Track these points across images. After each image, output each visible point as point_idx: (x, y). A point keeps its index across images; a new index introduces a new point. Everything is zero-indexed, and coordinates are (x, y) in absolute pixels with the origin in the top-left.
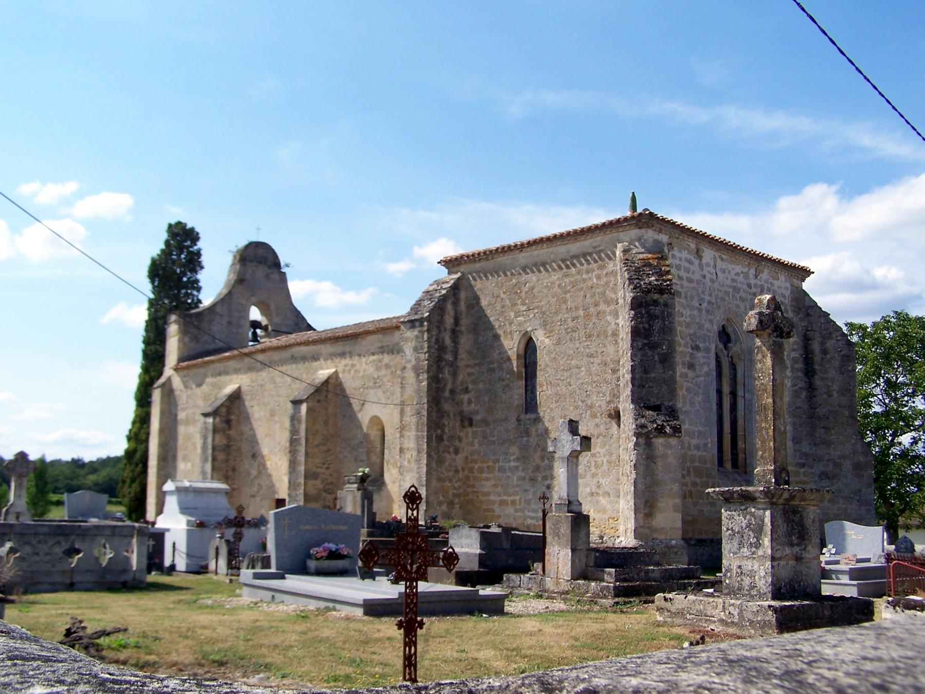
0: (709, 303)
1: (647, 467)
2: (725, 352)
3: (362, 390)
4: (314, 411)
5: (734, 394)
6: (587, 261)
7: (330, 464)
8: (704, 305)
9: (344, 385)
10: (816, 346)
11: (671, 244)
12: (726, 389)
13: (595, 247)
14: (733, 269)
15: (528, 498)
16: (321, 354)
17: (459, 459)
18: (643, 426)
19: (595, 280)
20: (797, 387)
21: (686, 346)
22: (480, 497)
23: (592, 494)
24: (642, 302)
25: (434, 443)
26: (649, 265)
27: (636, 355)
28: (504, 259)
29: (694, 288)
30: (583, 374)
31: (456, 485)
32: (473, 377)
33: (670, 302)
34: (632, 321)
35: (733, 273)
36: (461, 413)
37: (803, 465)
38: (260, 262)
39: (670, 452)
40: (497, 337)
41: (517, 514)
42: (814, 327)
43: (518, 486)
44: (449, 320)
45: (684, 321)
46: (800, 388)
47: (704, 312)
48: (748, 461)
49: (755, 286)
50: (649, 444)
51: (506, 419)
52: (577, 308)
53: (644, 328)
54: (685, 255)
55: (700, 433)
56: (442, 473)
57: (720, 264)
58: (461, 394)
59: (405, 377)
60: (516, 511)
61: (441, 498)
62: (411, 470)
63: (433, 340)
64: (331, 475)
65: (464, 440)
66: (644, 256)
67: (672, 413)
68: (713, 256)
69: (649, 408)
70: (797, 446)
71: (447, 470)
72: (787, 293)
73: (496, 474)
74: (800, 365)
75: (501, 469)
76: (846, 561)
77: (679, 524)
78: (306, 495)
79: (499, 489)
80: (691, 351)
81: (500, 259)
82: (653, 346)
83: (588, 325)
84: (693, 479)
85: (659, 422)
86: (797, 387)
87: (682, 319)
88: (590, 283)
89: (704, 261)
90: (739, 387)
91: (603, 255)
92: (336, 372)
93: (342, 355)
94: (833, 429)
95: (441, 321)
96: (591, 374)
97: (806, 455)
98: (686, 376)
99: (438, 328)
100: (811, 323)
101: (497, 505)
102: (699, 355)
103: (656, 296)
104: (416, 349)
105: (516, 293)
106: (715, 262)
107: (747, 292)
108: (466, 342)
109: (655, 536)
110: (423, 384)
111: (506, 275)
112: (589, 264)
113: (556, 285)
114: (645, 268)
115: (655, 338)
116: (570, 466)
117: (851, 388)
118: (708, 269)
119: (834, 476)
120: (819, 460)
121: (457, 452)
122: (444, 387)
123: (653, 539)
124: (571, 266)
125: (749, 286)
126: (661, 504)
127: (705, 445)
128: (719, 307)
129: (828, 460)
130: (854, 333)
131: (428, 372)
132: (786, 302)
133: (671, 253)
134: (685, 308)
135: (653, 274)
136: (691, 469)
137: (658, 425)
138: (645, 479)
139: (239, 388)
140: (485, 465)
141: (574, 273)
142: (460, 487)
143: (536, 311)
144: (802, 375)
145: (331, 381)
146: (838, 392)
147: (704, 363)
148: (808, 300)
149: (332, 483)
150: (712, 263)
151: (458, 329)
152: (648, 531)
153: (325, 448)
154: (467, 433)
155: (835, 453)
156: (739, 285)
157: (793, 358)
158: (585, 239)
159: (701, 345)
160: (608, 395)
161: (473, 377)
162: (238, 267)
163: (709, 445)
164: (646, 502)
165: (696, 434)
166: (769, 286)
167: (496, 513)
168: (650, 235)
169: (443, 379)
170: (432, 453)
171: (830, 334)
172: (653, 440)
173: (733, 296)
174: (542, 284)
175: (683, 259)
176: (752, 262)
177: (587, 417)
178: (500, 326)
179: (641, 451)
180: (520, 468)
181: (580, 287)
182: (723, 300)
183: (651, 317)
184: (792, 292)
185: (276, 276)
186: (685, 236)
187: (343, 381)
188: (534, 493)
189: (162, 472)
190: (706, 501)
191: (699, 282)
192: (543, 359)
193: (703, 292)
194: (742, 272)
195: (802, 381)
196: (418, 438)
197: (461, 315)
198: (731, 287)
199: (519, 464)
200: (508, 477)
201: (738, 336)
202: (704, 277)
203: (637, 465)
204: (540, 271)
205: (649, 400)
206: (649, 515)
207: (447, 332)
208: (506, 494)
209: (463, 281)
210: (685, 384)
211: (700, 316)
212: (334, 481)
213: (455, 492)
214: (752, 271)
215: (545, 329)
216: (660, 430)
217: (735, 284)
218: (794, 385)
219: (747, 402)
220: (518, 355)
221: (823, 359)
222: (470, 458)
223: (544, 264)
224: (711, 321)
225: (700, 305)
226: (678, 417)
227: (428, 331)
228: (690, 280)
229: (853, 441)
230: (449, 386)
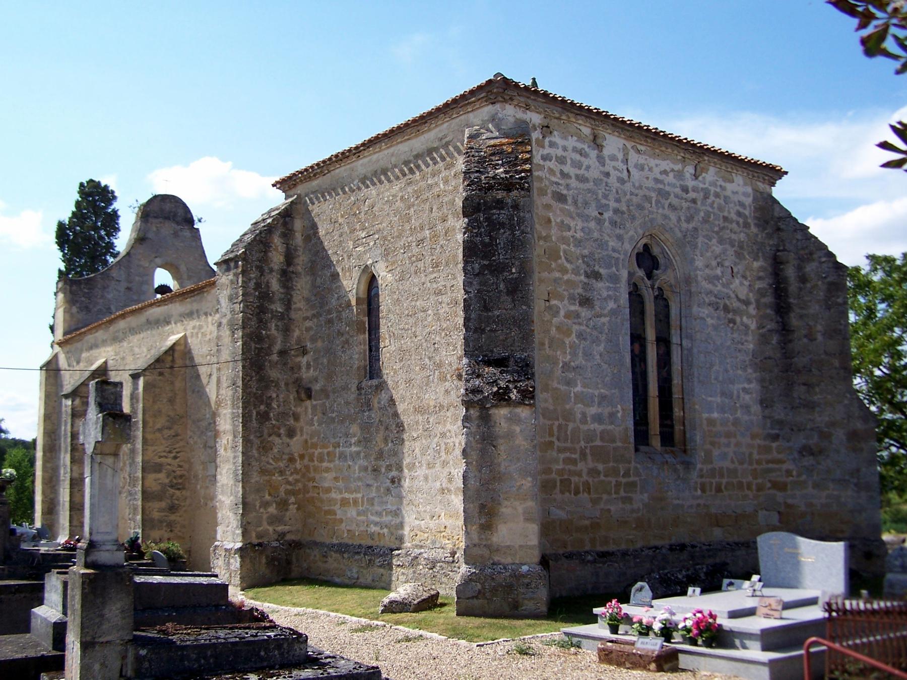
0: (616, 211)
1: (483, 452)
2: (649, 283)
3: (208, 357)
4: (154, 386)
5: (664, 341)
6: (433, 159)
7: (178, 452)
8: (606, 215)
9: (193, 352)
10: (790, 272)
11: (547, 127)
12: (651, 335)
13: (441, 139)
14: (657, 165)
15: (371, 496)
16: (172, 315)
17: (296, 445)
18: (476, 391)
19: (442, 186)
20: (765, 330)
21: (576, 272)
22: (321, 494)
23: (442, 491)
24: (479, 204)
25: (254, 424)
26: (501, 153)
27: (471, 283)
28: (341, 171)
29: (589, 191)
30: (430, 319)
31: (291, 479)
32: (312, 333)
33: (522, 201)
34: (465, 233)
35: (656, 171)
36: (298, 382)
37: (776, 438)
38: (167, 218)
39: (518, 429)
40: (335, 276)
41: (359, 518)
42: (788, 246)
43: (359, 479)
44: (277, 258)
45: (573, 237)
46: (769, 331)
47: (607, 224)
48: (688, 435)
49: (695, 189)
50: (485, 418)
51: (345, 388)
52: (422, 228)
53: (482, 242)
54: (572, 142)
55: (603, 398)
56: (268, 463)
57: (633, 157)
58: (297, 356)
59: (221, 336)
60: (359, 514)
61: (267, 497)
62: (228, 461)
63: (252, 284)
64: (180, 466)
65: (302, 417)
66: (497, 141)
67: (525, 369)
68: (621, 146)
69: (488, 363)
70: (767, 412)
71: (276, 459)
72: (748, 201)
73: (337, 462)
74: (769, 299)
75: (342, 456)
76: (766, 611)
77: (534, 540)
78: (144, 492)
79: (340, 484)
80: (586, 280)
81: (337, 171)
82: (498, 269)
83: (435, 249)
84: (591, 465)
85: (502, 384)
86: (765, 330)
87: (569, 234)
88: (436, 190)
89: (606, 152)
90: (673, 331)
91: (451, 148)
92: (185, 337)
93: (190, 315)
94: (818, 385)
95: (265, 259)
96: (439, 319)
97: (781, 423)
98: (578, 316)
99: (261, 270)
100: (783, 241)
101: (338, 506)
102: (600, 285)
103: (500, 195)
104: (231, 299)
105: (355, 214)
106: (626, 155)
107: (682, 198)
108: (302, 286)
109: (496, 559)
110: (238, 344)
111: (344, 193)
112: (435, 163)
113: (398, 198)
114: (493, 158)
115: (501, 257)
116: (97, 474)
117: (842, 327)
118: (613, 163)
119: (821, 452)
120: (799, 430)
121: (291, 433)
122: (269, 348)
123: (493, 564)
124: (415, 170)
125: (685, 190)
126: (505, 510)
127: (612, 415)
128: (633, 218)
129: (812, 429)
130: (878, 267)
131: (244, 328)
132: (747, 212)
133: (547, 140)
134: (572, 217)
135: (502, 165)
136: (588, 451)
137: (500, 388)
138: (480, 471)
139: (106, 362)
140: (326, 451)
141: (418, 178)
142: (297, 481)
143: (377, 236)
144: (772, 313)
145: (177, 348)
146: (824, 335)
147: (609, 297)
148: (777, 209)
149: (181, 477)
150: (620, 156)
151: (291, 269)
152: (486, 552)
153: (172, 432)
154: (306, 408)
155: (821, 418)
156: (667, 188)
157: (759, 289)
158: (429, 130)
159: (602, 271)
160: (459, 347)
161: (312, 333)
162: (139, 224)
163: (619, 415)
164: (482, 506)
165: (596, 399)
166: (718, 190)
167: (338, 517)
168: (510, 113)
169: (268, 336)
170: (252, 437)
171: (811, 254)
172: (491, 412)
173: (658, 202)
174: (383, 198)
175: (570, 148)
176: (687, 156)
177: (436, 380)
178: (338, 261)
179: (474, 429)
180: (362, 455)
181: (425, 197)
182: (640, 207)
183: (494, 226)
184: (755, 199)
185: (187, 233)
186: (571, 115)
187: (192, 347)
188: (378, 488)
189: (49, 465)
190: (614, 496)
191: (597, 182)
192: (385, 302)
193: (606, 197)
194: (672, 170)
195: (772, 320)
196: (234, 417)
197: (296, 250)
198: (654, 190)
199: (361, 449)
200: (349, 466)
201: (669, 259)
202: (607, 175)
203: (468, 450)
204: (381, 182)
205: (492, 351)
206: (487, 527)
207: (274, 273)
208: (348, 490)
209: (299, 206)
210: (576, 328)
211: (600, 230)
212: (185, 473)
213: (289, 487)
214: (690, 170)
215: (387, 260)
216: (502, 397)
217: (661, 186)
218: (760, 327)
219: (685, 352)
220: (358, 299)
221: (800, 289)
222: (309, 442)
223: (384, 172)
224: (620, 238)
225: (601, 214)
226: (533, 374)
227: (243, 272)
228: (582, 179)
229: (846, 402)
230: (277, 347)
